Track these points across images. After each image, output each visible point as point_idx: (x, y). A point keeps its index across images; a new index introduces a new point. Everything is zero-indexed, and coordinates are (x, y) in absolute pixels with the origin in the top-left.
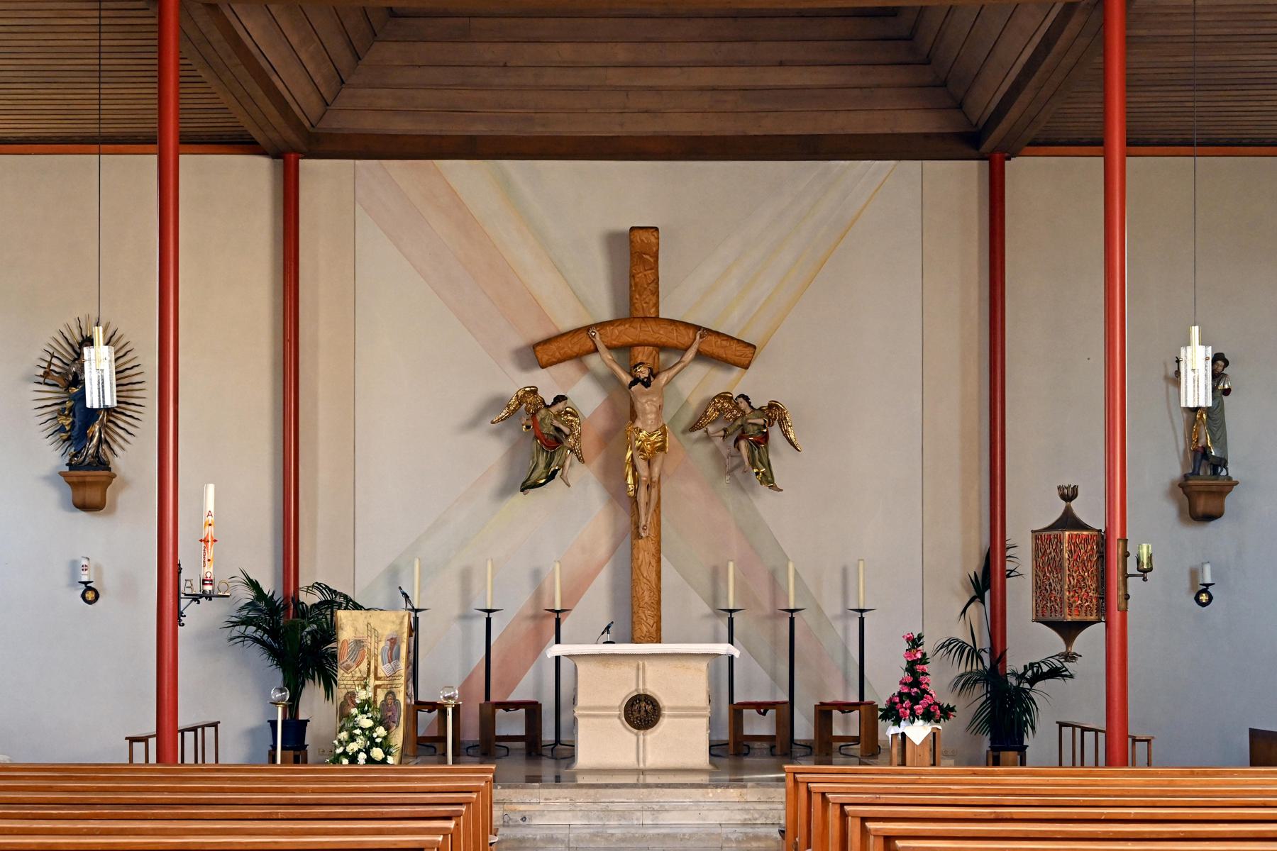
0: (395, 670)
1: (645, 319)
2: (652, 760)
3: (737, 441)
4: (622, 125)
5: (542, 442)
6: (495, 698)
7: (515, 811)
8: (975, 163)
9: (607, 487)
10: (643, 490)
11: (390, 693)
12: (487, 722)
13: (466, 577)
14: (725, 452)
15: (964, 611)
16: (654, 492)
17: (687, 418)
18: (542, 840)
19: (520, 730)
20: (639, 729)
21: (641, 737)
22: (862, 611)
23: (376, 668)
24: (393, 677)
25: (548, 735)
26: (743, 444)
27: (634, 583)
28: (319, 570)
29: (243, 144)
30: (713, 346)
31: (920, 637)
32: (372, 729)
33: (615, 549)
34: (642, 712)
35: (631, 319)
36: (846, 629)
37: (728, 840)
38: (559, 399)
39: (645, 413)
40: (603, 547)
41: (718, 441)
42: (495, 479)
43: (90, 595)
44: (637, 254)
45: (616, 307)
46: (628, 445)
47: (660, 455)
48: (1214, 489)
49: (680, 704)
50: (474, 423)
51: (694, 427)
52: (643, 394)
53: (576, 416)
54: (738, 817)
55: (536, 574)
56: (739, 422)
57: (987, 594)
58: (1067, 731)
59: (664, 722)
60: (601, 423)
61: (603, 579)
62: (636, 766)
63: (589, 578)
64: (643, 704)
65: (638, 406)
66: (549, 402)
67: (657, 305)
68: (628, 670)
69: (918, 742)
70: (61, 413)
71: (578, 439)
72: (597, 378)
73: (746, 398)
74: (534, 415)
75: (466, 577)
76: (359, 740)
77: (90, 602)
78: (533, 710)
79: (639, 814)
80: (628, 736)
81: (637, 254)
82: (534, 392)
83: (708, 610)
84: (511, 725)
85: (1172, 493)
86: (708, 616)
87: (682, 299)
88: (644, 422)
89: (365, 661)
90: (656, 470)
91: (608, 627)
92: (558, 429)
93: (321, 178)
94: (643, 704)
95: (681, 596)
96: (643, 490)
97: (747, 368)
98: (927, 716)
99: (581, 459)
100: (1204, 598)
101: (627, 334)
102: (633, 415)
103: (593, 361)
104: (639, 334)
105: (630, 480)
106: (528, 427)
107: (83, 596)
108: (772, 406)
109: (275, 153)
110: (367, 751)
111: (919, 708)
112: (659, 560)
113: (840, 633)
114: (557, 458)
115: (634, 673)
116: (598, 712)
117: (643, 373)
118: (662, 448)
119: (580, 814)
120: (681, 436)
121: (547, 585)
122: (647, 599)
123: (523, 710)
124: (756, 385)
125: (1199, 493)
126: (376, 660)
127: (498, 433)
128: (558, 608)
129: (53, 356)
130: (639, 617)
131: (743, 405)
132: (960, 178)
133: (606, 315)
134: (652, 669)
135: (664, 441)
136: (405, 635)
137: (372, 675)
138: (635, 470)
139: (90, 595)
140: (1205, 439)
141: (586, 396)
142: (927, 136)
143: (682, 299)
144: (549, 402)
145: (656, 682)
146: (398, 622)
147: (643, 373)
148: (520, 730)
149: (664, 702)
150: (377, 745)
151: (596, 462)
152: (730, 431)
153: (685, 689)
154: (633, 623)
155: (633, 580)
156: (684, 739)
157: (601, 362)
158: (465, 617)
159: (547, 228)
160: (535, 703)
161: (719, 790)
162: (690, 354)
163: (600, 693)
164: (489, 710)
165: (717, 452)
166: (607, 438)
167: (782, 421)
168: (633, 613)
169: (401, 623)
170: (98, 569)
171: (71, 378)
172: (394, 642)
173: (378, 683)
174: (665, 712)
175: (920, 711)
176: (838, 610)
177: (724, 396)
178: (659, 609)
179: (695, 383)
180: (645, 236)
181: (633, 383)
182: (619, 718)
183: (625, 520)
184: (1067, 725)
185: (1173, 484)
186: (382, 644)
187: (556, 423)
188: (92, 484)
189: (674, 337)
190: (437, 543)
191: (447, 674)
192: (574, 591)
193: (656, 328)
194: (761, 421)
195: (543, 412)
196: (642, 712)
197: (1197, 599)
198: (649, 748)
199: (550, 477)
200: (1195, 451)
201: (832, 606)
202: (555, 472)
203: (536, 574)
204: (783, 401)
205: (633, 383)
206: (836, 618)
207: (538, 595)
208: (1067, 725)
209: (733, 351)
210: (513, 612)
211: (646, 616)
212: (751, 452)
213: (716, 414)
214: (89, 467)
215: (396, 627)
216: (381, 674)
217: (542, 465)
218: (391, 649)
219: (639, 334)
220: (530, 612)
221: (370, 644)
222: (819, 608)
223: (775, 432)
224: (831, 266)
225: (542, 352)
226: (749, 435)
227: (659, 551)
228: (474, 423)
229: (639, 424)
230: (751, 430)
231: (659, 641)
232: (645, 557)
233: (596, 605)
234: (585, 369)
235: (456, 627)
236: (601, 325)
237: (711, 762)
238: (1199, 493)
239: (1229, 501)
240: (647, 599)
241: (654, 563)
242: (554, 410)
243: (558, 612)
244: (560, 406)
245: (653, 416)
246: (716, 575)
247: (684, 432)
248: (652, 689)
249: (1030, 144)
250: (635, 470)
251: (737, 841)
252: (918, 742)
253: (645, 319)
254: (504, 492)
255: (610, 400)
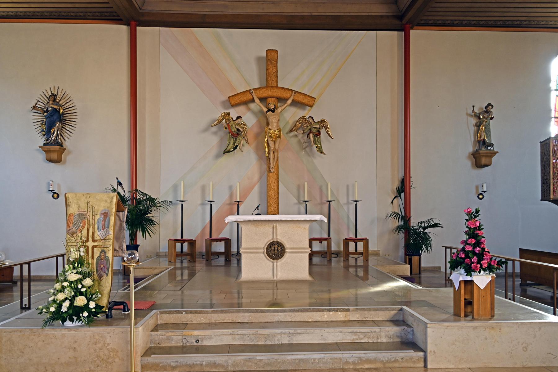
0: (107, 234)
1: (272, 87)
2: (281, 275)
3: (308, 135)
4: (263, 9)
5: (234, 134)
6: (214, 237)
7: (191, 336)
8: (396, 32)
9: (258, 154)
10: (272, 153)
11: (103, 251)
12: (209, 246)
13: (203, 189)
14: (302, 141)
15: (392, 202)
16: (276, 154)
17: (288, 128)
18: (207, 365)
19: (223, 250)
20: (274, 259)
21: (275, 263)
22: (356, 201)
23: (93, 234)
24: (105, 240)
25: (234, 249)
26: (311, 135)
27: (268, 190)
28: (146, 188)
29: (112, 17)
30: (299, 98)
31: (477, 211)
32: (80, 281)
33: (260, 178)
34: (275, 251)
35: (267, 87)
36: (348, 209)
37: (347, 362)
38: (239, 118)
39: (272, 122)
40: (256, 177)
41: (300, 136)
42: (215, 151)
43: (55, 196)
44: (270, 61)
45: (260, 81)
46: (266, 136)
47: (279, 139)
48: (489, 155)
49: (295, 247)
50: (206, 130)
51: (291, 131)
52: (272, 115)
53: (245, 125)
54: (348, 337)
55: (231, 187)
56: (309, 128)
57: (403, 194)
58: (448, 250)
59: (287, 255)
60: (256, 130)
61: (256, 189)
62: (272, 279)
63: (252, 188)
64: (276, 246)
65: (270, 120)
66: (234, 119)
67: (277, 82)
68: (268, 229)
69: (482, 287)
70: (42, 124)
71: (246, 135)
72: (254, 113)
73: (312, 118)
74: (228, 124)
75: (203, 189)
76: (66, 291)
77: (55, 199)
78: (227, 241)
79: (279, 336)
80: (269, 263)
81: (270, 61)
82: (229, 114)
83: (296, 201)
84: (220, 247)
85: (469, 157)
86: (296, 204)
87: (287, 79)
88: (272, 126)
89: (86, 228)
90: (277, 145)
91: (258, 207)
92: (238, 130)
93: (144, 33)
94: (276, 246)
95: (286, 196)
96: (272, 153)
97: (311, 106)
98: (490, 269)
99: (247, 142)
100: (481, 196)
101: (265, 93)
102: (268, 124)
103: (252, 106)
104: (270, 96)
105: (267, 150)
106: (226, 128)
107: (53, 196)
108: (322, 121)
109: (128, 24)
110: (72, 300)
111: (485, 263)
112: (278, 182)
113: (346, 210)
114: (237, 141)
115: (271, 230)
116: (253, 250)
117: (272, 107)
118: (279, 137)
119: (237, 337)
120: (286, 135)
121: (234, 191)
122: (273, 197)
123: (224, 242)
124: (316, 114)
125: (483, 156)
126: (93, 228)
127: (215, 133)
128: (238, 200)
129: (38, 101)
130: (270, 205)
131: (311, 120)
132: (392, 38)
133: (257, 86)
134: (280, 228)
135: (280, 134)
136: (114, 210)
137: (90, 239)
138: (269, 145)
139: (55, 196)
140: (484, 136)
141: (249, 118)
142: (382, 16)
143: (287, 79)
144: (234, 119)
145: (282, 235)
146: (109, 201)
147: (272, 107)
148: (223, 250)
149: (287, 245)
150: (81, 294)
151: (254, 145)
152: (306, 131)
153: (297, 240)
154: (268, 206)
155: (268, 189)
156: (296, 266)
157: (256, 106)
158: (203, 204)
159: (237, 53)
160: (228, 239)
161: (331, 313)
162: (289, 101)
163: (253, 242)
164: (212, 240)
165: (299, 141)
166: (257, 136)
167: (326, 126)
168: (268, 202)
169: (111, 202)
170: (59, 186)
171: (45, 110)
172: (106, 215)
173: (95, 244)
174: (287, 250)
175: (486, 265)
176: (345, 201)
177: (303, 118)
178: (278, 201)
179: (290, 115)
180: (273, 54)
181: (268, 111)
182: (263, 253)
183: (265, 167)
184: (449, 248)
185: (469, 153)
186: (98, 217)
187: (237, 127)
188: (54, 151)
189: (284, 94)
190: (194, 178)
191: (195, 229)
192: (245, 194)
193: (277, 91)
194: (318, 126)
195: (232, 122)
196: (275, 251)
197: (478, 197)
198: (279, 269)
199: (235, 148)
200: (479, 142)
201: (343, 200)
202: (237, 146)
203: (231, 187)
204: (326, 119)
205: (268, 111)
206: (345, 204)
207: (231, 195)
208: (449, 248)
209: (306, 100)
210: (221, 201)
211: (273, 203)
212: (315, 139)
213: (300, 125)
214: (52, 144)
215: (107, 205)
216: (97, 237)
217: (232, 143)
218: (104, 220)
219: (270, 96)
220: (228, 202)
221: (90, 216)
222: (338, 201)
223: (323, 131)
224: (343, 72)
225: (235, 101)
226: (313, 132)
227: (278, 178)
228: (206, 130)
229: (270, 127)
230: (314, 130)
231: (278, 214)
232: (272, 180)
233: (253, 199)
234: (249, 109)
235: (200, 208)
236: (255, 89)
237: (310, 273)
238: (483, 156)
239: (494, 159)
240: (273, 197)
241: (276, 182)
242: (236, 122)
243: (238, 202)
244: (239, 120)
245: (276, 124)
246: (300, 188)
247: (287, 133)
248: (280, 238)
249: (416, 25)
250: (269, 145)
251: (354, 363)
252: (482, 287)
253: (272, 87)
254: (218, 156)
255: (259, 121)
